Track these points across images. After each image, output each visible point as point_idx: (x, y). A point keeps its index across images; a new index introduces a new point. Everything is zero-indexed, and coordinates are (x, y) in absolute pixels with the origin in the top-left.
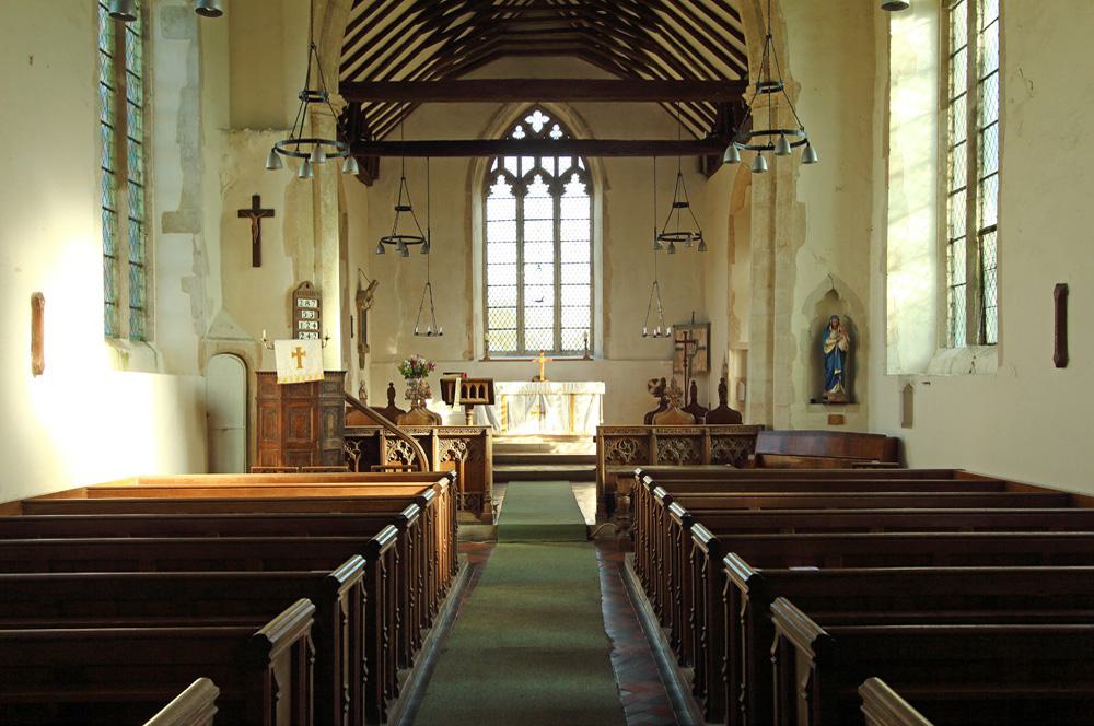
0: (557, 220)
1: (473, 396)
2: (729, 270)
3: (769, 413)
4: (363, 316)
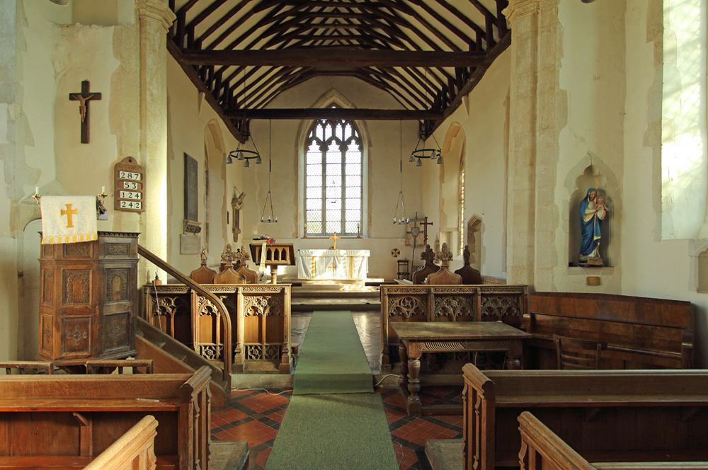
0: (343, 164)
1: (276, 258)
2: (441, 186)
3: (531, 274)
4: (236, 213)
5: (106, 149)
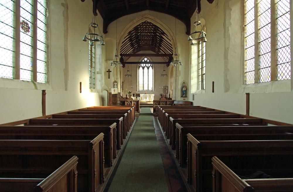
5: (112, 79)
